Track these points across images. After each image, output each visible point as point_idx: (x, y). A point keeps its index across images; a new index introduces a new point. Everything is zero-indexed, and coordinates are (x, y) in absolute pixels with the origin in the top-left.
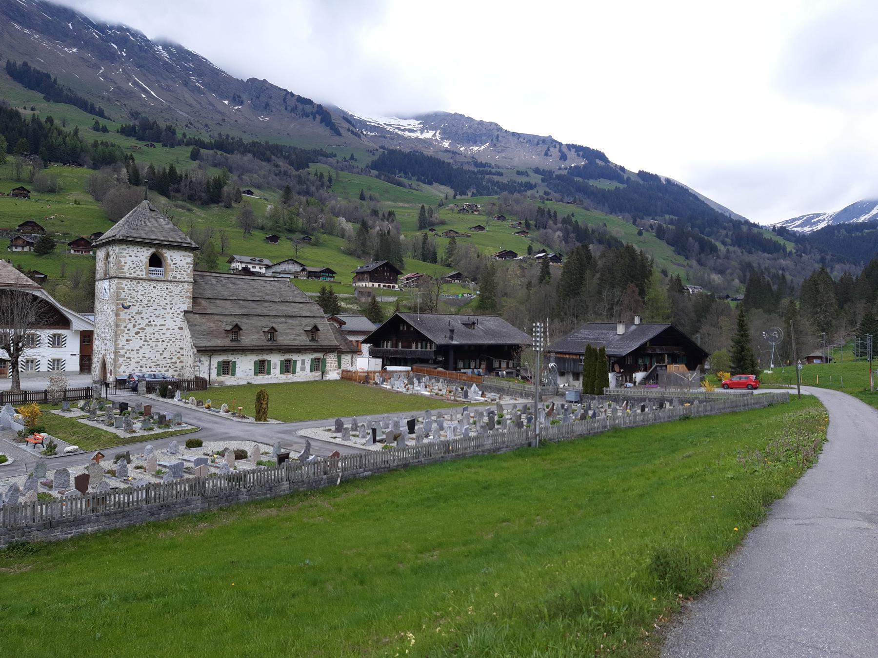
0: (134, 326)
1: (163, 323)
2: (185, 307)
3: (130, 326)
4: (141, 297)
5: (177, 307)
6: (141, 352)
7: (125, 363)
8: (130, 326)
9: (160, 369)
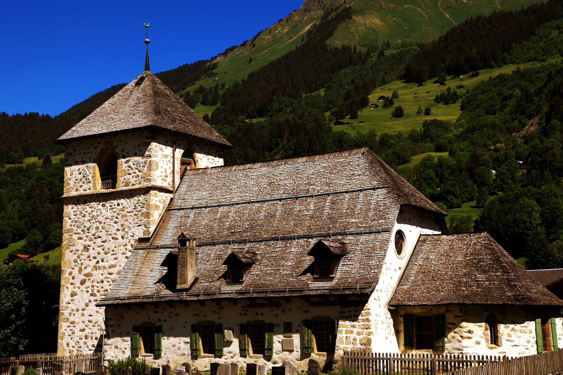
0: (80, 270)
1: (113, 262)
3: (75, 272)
4: (88, 225)
6: (86, 313)
7: (68, 332)
8: (75, 272)
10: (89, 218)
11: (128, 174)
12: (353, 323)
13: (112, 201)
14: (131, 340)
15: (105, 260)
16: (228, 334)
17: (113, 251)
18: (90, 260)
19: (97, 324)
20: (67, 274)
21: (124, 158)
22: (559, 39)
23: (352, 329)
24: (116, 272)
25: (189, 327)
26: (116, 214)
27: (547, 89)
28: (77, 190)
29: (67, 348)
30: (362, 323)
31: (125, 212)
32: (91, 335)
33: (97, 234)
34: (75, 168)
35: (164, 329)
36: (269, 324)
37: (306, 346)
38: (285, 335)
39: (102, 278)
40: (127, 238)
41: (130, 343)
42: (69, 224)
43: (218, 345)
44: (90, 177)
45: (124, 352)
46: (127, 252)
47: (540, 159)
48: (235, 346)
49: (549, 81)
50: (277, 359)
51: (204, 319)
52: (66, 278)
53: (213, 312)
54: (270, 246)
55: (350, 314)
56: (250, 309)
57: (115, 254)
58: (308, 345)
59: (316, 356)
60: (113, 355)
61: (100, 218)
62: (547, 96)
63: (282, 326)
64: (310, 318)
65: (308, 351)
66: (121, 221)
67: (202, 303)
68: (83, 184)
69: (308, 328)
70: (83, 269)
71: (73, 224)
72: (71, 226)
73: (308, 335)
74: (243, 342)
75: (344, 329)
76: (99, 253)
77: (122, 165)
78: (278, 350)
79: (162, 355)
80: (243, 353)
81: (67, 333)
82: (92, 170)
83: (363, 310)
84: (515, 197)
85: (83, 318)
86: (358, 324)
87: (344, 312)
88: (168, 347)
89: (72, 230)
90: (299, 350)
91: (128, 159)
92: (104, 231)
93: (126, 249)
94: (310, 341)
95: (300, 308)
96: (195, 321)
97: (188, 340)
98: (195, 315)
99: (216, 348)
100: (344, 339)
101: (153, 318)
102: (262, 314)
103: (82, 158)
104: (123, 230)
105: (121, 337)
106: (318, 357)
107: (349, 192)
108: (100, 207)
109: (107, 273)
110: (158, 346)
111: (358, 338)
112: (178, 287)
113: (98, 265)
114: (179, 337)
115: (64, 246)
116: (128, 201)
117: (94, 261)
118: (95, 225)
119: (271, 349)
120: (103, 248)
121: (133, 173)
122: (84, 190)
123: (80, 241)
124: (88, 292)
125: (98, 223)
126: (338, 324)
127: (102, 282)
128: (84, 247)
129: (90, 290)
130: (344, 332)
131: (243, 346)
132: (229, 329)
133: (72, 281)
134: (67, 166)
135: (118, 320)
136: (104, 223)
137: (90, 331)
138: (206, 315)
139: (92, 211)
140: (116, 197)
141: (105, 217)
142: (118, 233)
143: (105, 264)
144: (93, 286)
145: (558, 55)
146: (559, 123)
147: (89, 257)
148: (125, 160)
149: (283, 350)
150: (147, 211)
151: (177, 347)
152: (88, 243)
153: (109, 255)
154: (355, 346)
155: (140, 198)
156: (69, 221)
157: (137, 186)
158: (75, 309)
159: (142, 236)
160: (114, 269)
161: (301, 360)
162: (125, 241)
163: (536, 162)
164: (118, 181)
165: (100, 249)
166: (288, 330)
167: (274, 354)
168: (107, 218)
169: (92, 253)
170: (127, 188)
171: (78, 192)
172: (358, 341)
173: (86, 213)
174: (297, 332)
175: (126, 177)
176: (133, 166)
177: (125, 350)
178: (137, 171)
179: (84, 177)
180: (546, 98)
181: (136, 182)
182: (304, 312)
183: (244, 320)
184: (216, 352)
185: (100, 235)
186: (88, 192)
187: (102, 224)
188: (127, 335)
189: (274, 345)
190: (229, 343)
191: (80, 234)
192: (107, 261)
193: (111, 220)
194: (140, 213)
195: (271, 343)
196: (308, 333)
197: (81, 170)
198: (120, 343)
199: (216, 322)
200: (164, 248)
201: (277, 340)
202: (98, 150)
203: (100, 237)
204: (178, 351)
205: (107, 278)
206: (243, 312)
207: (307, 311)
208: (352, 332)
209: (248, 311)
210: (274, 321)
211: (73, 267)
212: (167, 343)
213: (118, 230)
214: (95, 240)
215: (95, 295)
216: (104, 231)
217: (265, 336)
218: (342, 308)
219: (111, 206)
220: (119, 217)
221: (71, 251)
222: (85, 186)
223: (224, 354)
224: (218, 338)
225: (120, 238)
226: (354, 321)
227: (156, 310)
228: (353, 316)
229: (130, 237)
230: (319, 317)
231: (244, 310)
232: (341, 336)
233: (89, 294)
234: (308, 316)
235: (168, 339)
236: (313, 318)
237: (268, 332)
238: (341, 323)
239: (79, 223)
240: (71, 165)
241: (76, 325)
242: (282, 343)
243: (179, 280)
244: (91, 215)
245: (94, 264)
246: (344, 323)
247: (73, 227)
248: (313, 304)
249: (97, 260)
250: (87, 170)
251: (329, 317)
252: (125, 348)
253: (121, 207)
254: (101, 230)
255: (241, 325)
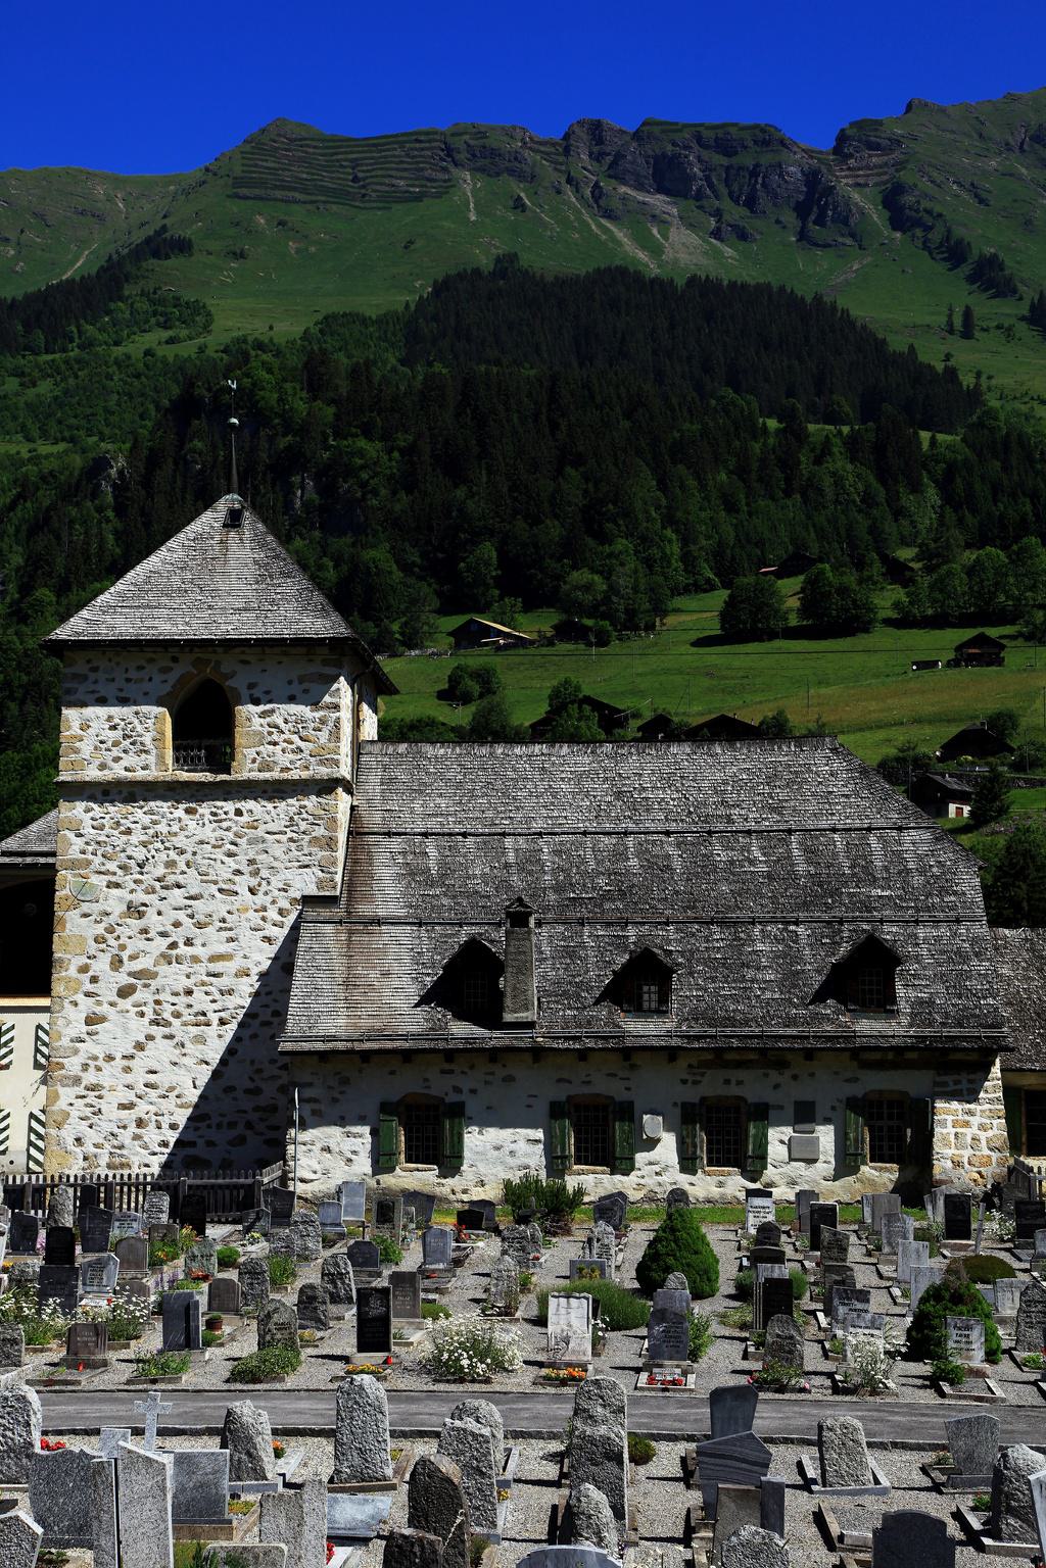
0: (117, 963)
1: (224, 948)
4: (140, 854)
8: (102, 965)
10: (144, 838)
11: (269, 743)
12: (968, 1106)
13: (219, 804)
16: (652, 1124)
18: (148, 939)
19: (176, 1093)
20: (72, 971)
21: (256, 702)
22: (22, 400)
23: (967, 1118)
25: (542, 1108)
26: (230, 835)
27: (19, 514)
28: (103, 767)
29: (78, 1150)
30: (988, 1106)
31: (260, 832)
32: (154, 1118)
33: (171, 879)
34: (97, 713)
35: (469, 1110)
36: (757, 1105)
37: (852, 1151)
38: (799, 1127)
39: (189, 983)
40: (266, 893)
41: (368, 1139)
42: (76, 848)
43: (623, 1148)
44: (147, 739)
46: (268, 926)
47: (25, 678)
49: (21, 497)
50: (776, 1179)
51: (586, 1090)
52: (69, 980)
53: (608, 1075)
55: (959, 1087)
56: (709, 1072)
57: (231, 929)
58: (857, 1148)
60: (317, 1167)
61: (180, 841)
62: (18, 531)
63: (790, 1111)
66: (246, 851)
67: (583, 1055)
68: (123, 755)
70: (125, 959)
71: (90, 848)
72: (83, 852)
75: (950, 1118)
76: (177, 924)
77: (249, 720)
78: (780, 1158)
80: (688, 1164)
81: (75, 1114)
82: (154, 722)
83: (986, 1080)
84: (22, 767)
85: (129, 1078)
86: (979, 1108)
87: (945, 1084)
88: (480, 1149)
89: (89, 863)
90: (833, 1160)
91: (269, 707)
92: (192, 872)
93: (264, 919)
96: (561, 1094)
97: (539, 1134)
98: (559, 1080)
99: (617, 1155)
100: (952, 1137)
101: (440, 1086)
102: (740, 1083)
103: (121, 690)
104: (256, 873)
106: (877, 1174)
108: (180, 813)
110: (453, 1147)
111: (983, 1136)
112: (508, 1017)
113: (174, 952)
114: (515, 1126)
115: (63, 902)
116: (270, 806)
117: (162, 944)
118: (163, 856)
119: (762, 1157)
120: (189, 911)
121: (285, 741)
122: (126, 769)
123: (115, 892)
124: (142, 1015)
125: (171, 852)
126: (934, 1108)
127: (189, 993)
128: (129, 908)
129: (149, 1010)
130: (949, 1124)
131: (691, 1149)
133: (89, 987)
134: (70, 705)
135: (329, 1087)
136: (194, 854)
137: (153, 1109)
139: (155, 823)
140: (229, 793)
141: (197, 838)
142: (237, 879)
143: (197, 950)
144: (158, 1002)
145: (20, 437)
146: (54, 599)
147: (145, 931)
148: (262, 708)
149: (791, 1159)
150: (327, 833)
151: (506, 1150)
152: (140, 897)
153: (210, 930)
154: (977, 1153)
155: (306, 803)
156: (79, 843)
157: (295, 775)
158: (101, 1056)
160: (227, 963)
162: (260, 899)
163: (16, 683)
164: (238, 756)
165: (181, 916)
166: (804, 1115)
169: (152, 919)
170: (267, 775)
171: (106, 772)
172: (984, 1142)
173: (133, 826)
174: (827, 1121)
175: (261, 748)
176: (283, 726)
177: (353, 1157)
178: (295, 738)
179: (125, 737)
180: (16, 535)
181: (291, 762)
183: (692, 1095)
185: (182, 882)
186: (140, 775)
187: (188, 856)
188: (361, 1121)
190: (652, 1143)
191: (115, 874)
192: (204, 945)
193: (214, 847)
194: (307, 838)
195: (762, 1144)
196: (857, 1124)
197: (117, 721)
198: (339, 1140)
201: (778, 1138)
202: (173, 677)
203: (179, 886)
205: (203, 984)
206: (690, 1078)
207: (856, 1080)
208: (967, 1124)
209: (703, 1075)
210: (770, 1097)
211: (92, 952)
212: (476, 1141)
213: (238, 872)
214: (164, 893)
215: (168, 1024)
216: (192, 872)
217: (747, 1131)
218: (939, 1075)
219: (214, 814)
220: (243, 841)
221: (86, 915)
222: (130, 760)
223: (637, 1165)
224: (623, 1131)
225: (244, 891)
226: (969, 1102)
227: (447, 1066)
228: (965, 1092)
229: (276, 893)
230: (881, 1092)
232: (944, 1131)
233: (146, 1020)
234: (858, 1090)
238: (939, 1104)
239: (109, 849)
240: (84, 705)
241: (103, 1092)
244: (151, 832)
245: (163, 949)
246: (947, 1105)
247: (90, 857)
249: (170, 940)
250: (136, 722)
251: (907, 1093)
253: (245, 818)
254: (185, 868)
255: (684, 1105)
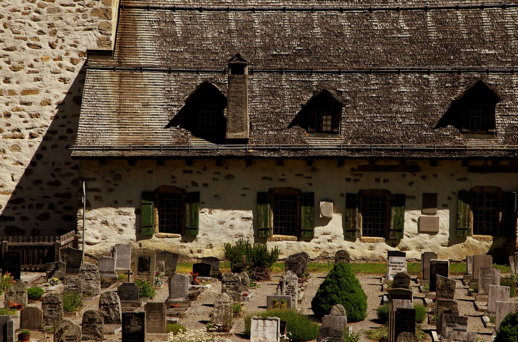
2: (90, 41)
5: (69, 40)
9: (26, 212)
14: (137, 212)
15: (13, 80)
17: (31, 66)
24: (40, 101)
25: (252, 196)
26: (35, 6)
35: (203, 197)
36: (397, 196)
37: (461, 226)
39: (8, 109)
40: (61, 48)
41: (133, 216)
45: (121, 230)
48: (336, 223)
54: (357, 81)
56: (365, 174)
58: (464, 225)
59: (475, 240)
60: (98, 234)
64: (468, 189)
65: (463, 233)
69: (465, 202)
73: (465, 212)
74: (351, 219)
79: (199, 236)
80: (350, 234)
92: (8, 31)
93: (60, 66)
94: (466, 220)
95: (452, 175)
96: (265, 187)
97: (250, 214)
98: (264, 178)
99: (302, 228)
102: (386, 181)
105: (116, 207)
106: (478, 242)
107: (460, 8)
109: (18, 101)
110: (191, 222)
112: (230, 135)
119: (400, 230)
120: (7, 59)
132: (327, 200)
135: (107, 181)
136: (9, 18)
138: (284, 180)
141: (11, 7)
142: (40, 37)
149: (420, 232)
150: (103, 6)
159: (94, 46)
160: (35, 96)
161: (448, 246)
162: (57, 52)
166: (430, 203)
167: (405, 237)
168: (14, 10)
177: (123, 228)
182: (460, 180)
183: (354, 188)
184: (302, 233)
188: (129, 204)
189: (405, 224)
190: (326, 221)
192: (18, 83)
194: (90, 9)
195: (400, 222)
198: (114, 216)
199: (303, 191)
200: (150, 71)
201: (411, 219)
204: (230, 231)
205: (18, 110)
206: (353, 177)
207: (466, 179)
210: (407, 190)
212: (208, 218)
213: (41, 32)
217: (390, 212)
220: (44, 10)
223: (315, 235)
227: (188, 168)
229: (69, 47)
230: (482, 188)
231: (355, 174)
234: (466, 186)
235: (210, 213)
236: (472, 189)
237: (396, 206)
242: (419, 222)
243: (230, 125)
248: (473, 170)
251: (500, 188)
252: (124, 225)
